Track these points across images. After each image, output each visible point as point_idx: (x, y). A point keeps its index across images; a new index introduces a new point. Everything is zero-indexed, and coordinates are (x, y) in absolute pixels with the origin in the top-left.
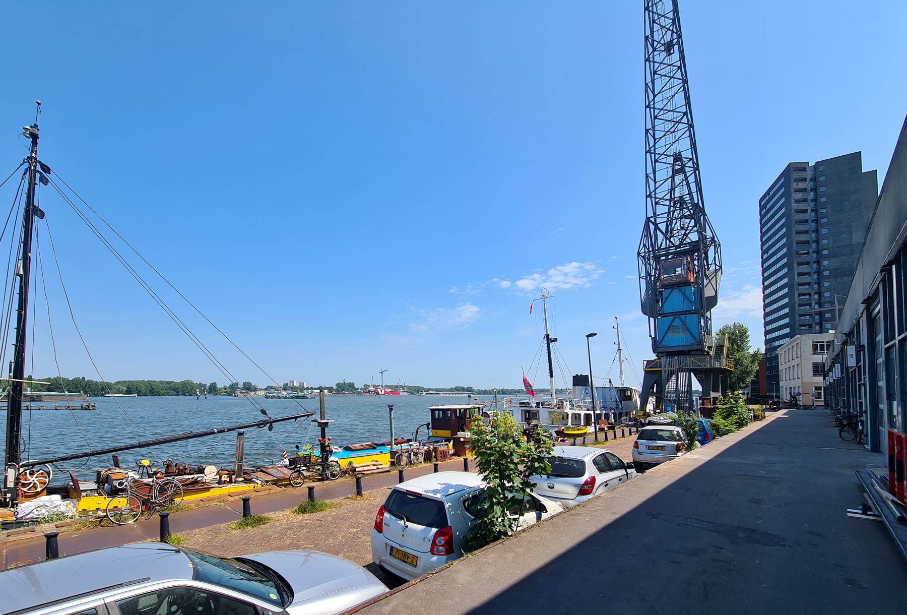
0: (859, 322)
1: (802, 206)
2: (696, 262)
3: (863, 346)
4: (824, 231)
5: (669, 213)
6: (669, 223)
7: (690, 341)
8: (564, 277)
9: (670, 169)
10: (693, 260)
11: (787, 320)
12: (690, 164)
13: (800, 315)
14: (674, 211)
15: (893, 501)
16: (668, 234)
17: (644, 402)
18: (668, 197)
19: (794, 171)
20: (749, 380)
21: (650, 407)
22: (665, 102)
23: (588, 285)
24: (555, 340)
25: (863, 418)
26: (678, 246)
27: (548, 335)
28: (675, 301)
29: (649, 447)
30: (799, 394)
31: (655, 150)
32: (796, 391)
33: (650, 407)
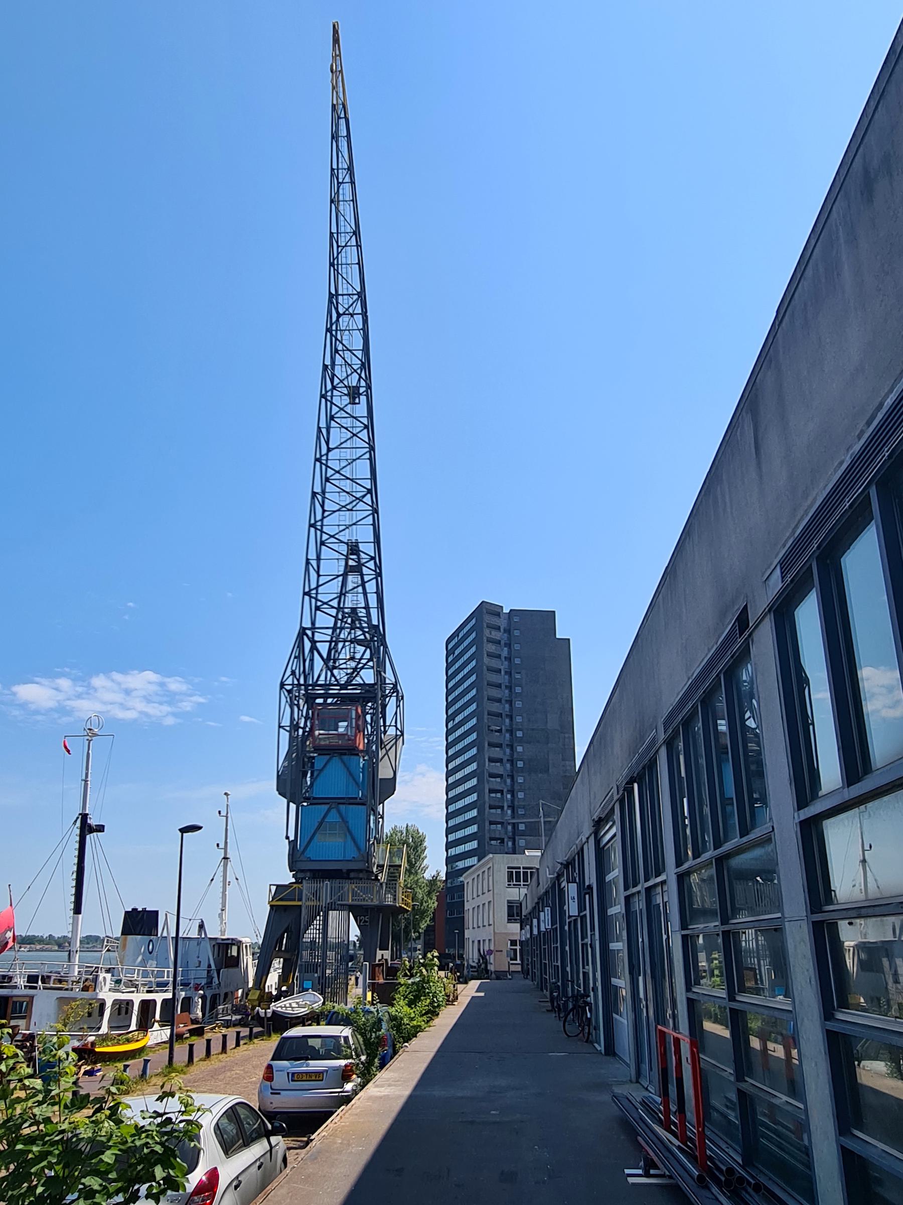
0: (582, 849)
1: (495, 663)
2: (368, 718)
3: (590, 887)
4: (518, 704)
5: (334, 628)
6: (334, 642)
7: (352, 853)
8: (124, 695)
9: (343, 563)
10: (365, 713)
11: (474, 829)
12: (371, 564)
13: (491, 823)
14: (342, 628)
15: (679, 1148)
16: (330, 662)
17: (263, 972)
18: (335, 603)
19: (485, 612)
20: (423, 925)
21: (273, 979)
22: (344, 463)
23: (170, 721)
24: (100, 829)
25: (591, 999)
26: (344, 687)
27: (84, 817)
28: (333, 780)
29: (294, 1077)
30: (490, 952)
31: (322, 526)
32: (487, 948)
33: (273, 979)
